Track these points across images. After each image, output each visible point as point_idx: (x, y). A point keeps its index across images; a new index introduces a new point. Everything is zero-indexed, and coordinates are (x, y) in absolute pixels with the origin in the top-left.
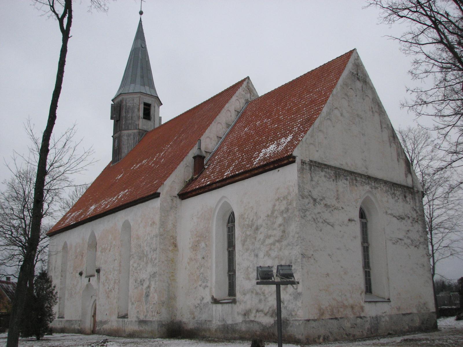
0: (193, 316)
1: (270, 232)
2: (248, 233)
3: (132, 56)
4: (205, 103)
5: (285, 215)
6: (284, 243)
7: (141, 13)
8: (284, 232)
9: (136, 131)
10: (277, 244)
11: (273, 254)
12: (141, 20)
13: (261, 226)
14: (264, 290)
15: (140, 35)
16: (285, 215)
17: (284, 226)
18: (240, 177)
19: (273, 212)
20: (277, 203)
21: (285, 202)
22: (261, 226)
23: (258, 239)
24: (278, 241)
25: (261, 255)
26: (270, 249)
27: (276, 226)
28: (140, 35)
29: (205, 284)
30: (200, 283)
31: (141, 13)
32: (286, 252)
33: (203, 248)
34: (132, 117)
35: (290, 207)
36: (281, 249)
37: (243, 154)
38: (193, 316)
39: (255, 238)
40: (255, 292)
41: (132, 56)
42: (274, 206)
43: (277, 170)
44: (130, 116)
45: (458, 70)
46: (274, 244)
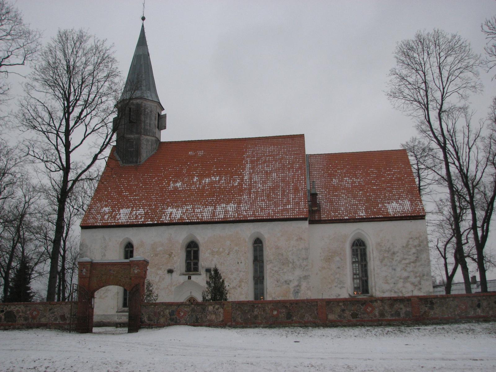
0: (210, 308)
1: (405, 257)
2: (386, 255)
3: (135, 59)
4: (259, 138)
5: (418, 248)
6: (418, 264)
7: (143, 19)
8: (417, 257)
9: (154, 138)
10: (412, 264)
11: (409, 269)
12: (143, 26)
13: (398, 252)
14: (402, 290)
15: (142, 42)
16: (418, 248)
17: (417, 254)
18: (379, 220)
19: (407, 245)
20: (411, 240)
21: (417, 241)
22: (398, 252)
23: (395, 260)
24: (413, 262)
25: (398, 269)
26: (407, 266)
27: (411, 253)
28: (142, 42)
29: (341, 285)
30: (335, 284)
31: (143, 19)
32: (420, 269)
34: (150, 124)
35: (421, 244)
36: (415, 267)
37: (215, 174)
38: (210, 308)
39: (393, 259)
40: (393, 291)
41: (135, 59)
42: (408, 241)
43: (411, 221)
44: (148, 123)
45: (103, 57)
46: (410, 264)
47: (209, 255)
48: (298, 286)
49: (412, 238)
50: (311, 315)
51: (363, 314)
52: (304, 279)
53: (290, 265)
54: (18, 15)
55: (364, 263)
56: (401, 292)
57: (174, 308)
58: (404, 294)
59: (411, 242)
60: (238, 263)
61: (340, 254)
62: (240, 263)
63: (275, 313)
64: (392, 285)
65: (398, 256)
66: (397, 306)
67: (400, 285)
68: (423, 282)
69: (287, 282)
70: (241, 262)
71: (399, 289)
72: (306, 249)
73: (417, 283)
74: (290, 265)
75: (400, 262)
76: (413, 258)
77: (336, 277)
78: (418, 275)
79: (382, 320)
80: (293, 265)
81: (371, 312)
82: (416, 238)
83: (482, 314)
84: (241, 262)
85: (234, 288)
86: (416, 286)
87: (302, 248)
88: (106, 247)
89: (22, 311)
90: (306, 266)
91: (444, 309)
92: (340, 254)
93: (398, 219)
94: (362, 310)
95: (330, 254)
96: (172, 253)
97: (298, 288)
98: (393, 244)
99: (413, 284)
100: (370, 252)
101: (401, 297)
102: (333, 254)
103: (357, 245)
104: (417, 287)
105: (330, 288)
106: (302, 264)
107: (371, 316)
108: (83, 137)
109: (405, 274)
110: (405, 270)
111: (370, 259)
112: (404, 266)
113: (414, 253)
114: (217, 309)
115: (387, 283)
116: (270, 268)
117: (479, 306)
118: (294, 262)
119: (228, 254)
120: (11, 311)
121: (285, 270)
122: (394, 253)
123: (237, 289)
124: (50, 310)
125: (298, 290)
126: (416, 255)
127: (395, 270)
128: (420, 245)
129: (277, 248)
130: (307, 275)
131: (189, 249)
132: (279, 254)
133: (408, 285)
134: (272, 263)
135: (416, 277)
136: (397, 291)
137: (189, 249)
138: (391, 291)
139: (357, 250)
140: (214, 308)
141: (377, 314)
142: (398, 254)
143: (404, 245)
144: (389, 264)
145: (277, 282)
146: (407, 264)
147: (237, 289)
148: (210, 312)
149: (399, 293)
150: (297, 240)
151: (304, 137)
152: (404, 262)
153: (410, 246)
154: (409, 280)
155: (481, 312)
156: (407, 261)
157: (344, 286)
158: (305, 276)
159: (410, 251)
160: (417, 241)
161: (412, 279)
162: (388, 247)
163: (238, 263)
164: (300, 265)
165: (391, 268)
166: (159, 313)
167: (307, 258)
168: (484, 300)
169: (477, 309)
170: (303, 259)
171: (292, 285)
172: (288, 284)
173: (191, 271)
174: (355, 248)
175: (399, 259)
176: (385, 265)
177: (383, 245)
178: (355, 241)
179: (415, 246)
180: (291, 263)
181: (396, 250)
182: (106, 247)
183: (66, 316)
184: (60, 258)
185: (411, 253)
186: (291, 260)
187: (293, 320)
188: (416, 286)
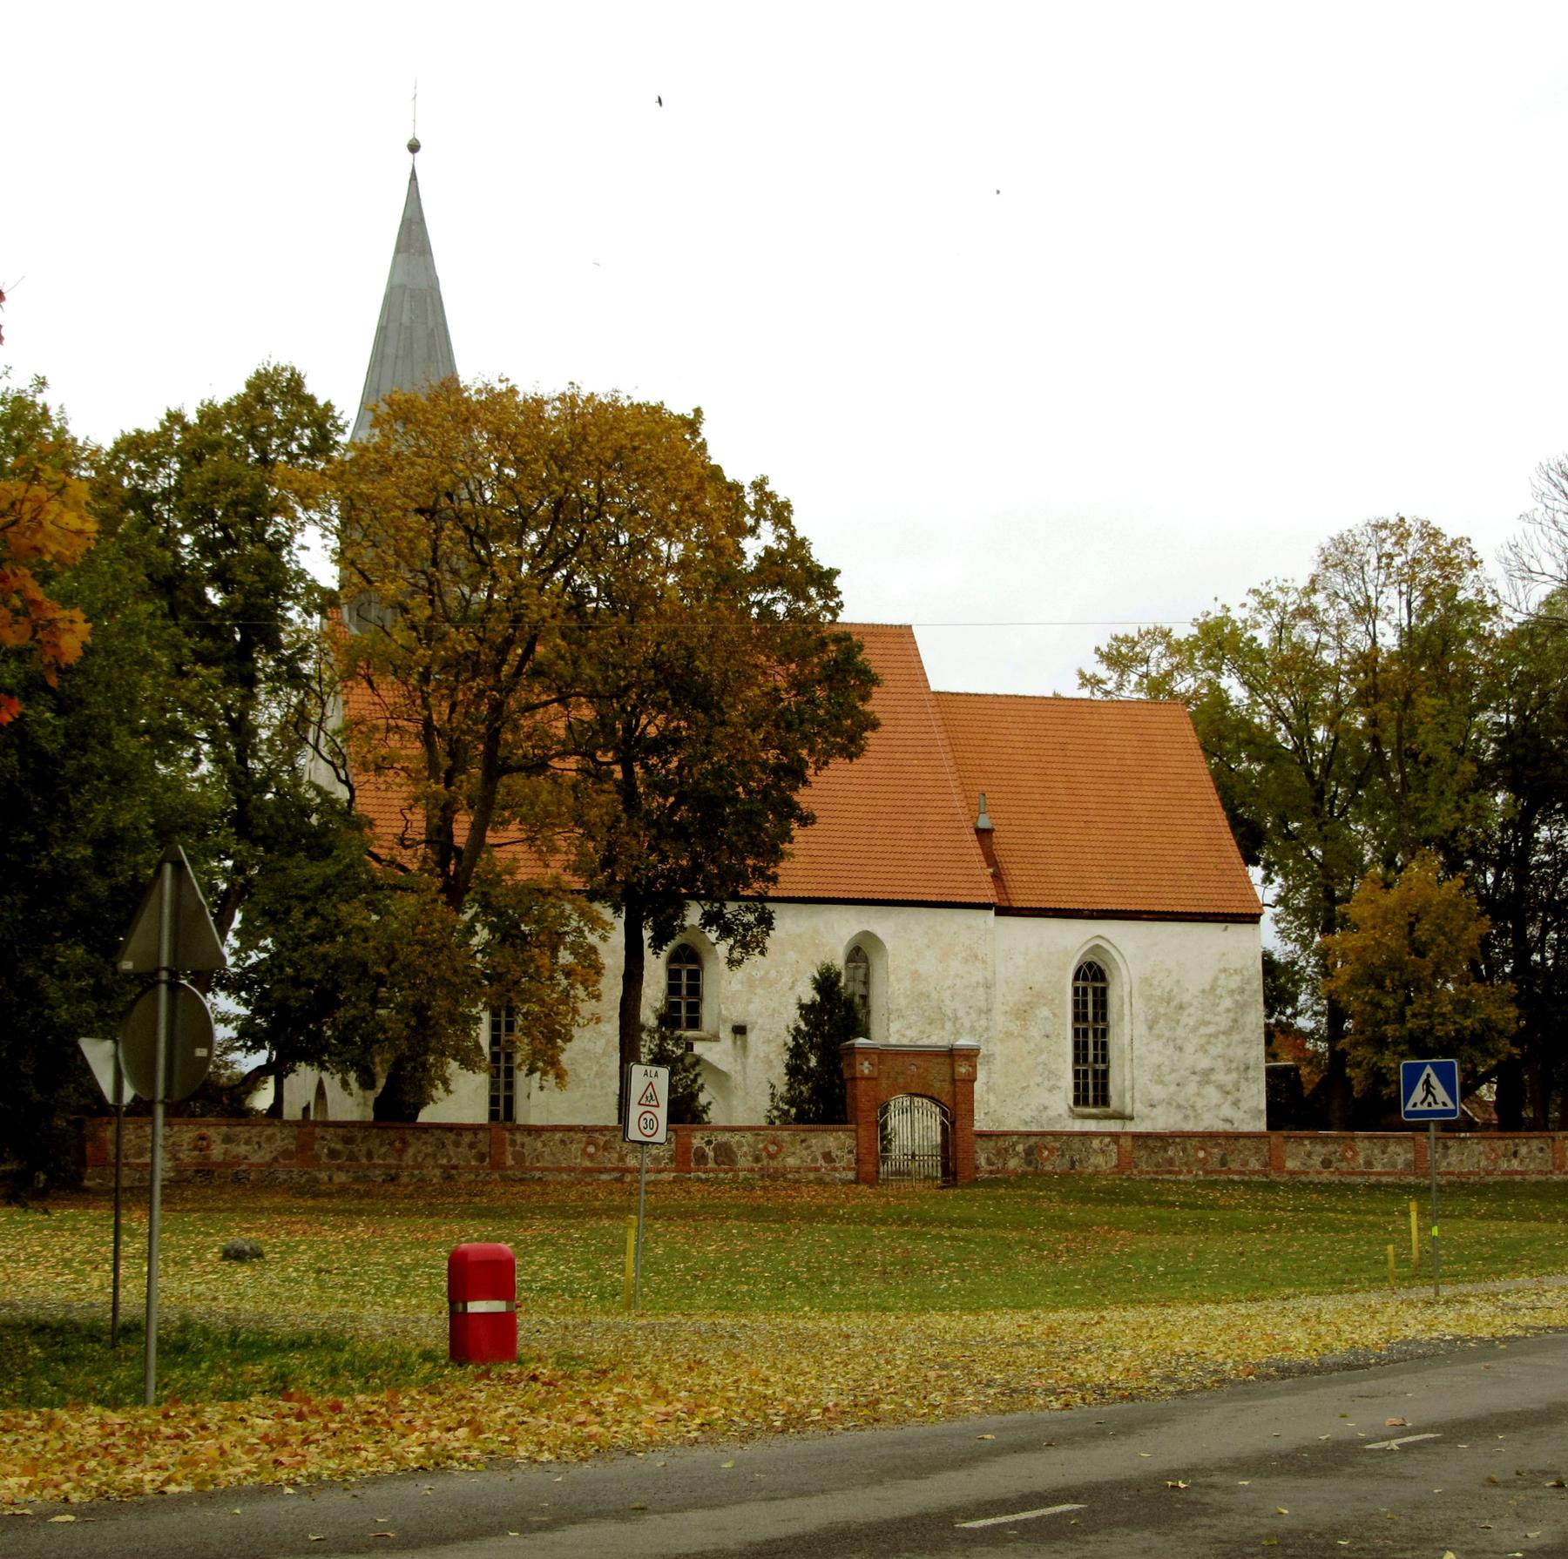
1: (1209, 1017)
2: (1161, 1010)
5: (1238, 998)
6: (1236, 1037)
10: (1222, 1037)
11: (1214, 1051)
20: (1223, 976)
21: (1237, 978)
25: (1190, 1049)
26: (1209, 1043)
29: (1052, 1083)
30: (1038, 1079)
33: (1047, 1018)
35: (1247, 987)
36: (1229, 1046)
42: (1216, 979)
46: (1216, 1035)
47: (739, 987)
49: (1225, 970)
51: (1341, 1161)
53: (948, 1025)
54: (616, 400)
55: (1100, 1026)
57: (1033, 1140)
59: (1222, 982)
61: (1052, 1000)
63: (1201, 1154)
64: (1173, 1088)
65: (1189, 1015)
67: (1192, 1088)
68: (1243, 1085)
71: (1188, 1100)
72: (988, 986)
73: (1229, 1087)
75: (1194, 1030)
76: (1225, 1022)
77: (1040, 1059)
78: (1234, 1065)
80: (954, 1024)
81: (1353, 1157)
82: (1236, 971)
86: (1228, 1093)
89: (748, 1142)
90: (987, 1029)
92: (1052, 1000)
95: (1028, 999)
98: (1178, 981)
99: (1220, 1087)
100: (1122, 998)
102: (1035, 1000)
103: (1085, 979)
104: (1229, 1097)
105: (1023, 1088)
106: (976, 1024)
109: (1204, 1063)
110: (1206, 1052)
111: (1122, 1018)
112: (1203, 1041)
113: (1228, 1010)
115: (1162, 1083)
117: (1515, 1154)
118: (956, 1018)
119: (791, 989)
120: (725, 1143)
122: (1181, 1007)
124: (803, 1141)
126: (1232, 1015)
127: (1181, 1049)
128: (1242, 991)
129: (916, 976)
131: (675, 966)
132: (921, 994)
133: (1211, 1092)
135: (1229, 1071)
136: (1183, 1103)
137: (675, 966)
138: (1169, 1104)
139: (1085, 990)
141: (1361, 1162)
142: (1191, 1010)
143: (1207, 987)
144: (1167, 1034)
146: (1210, 1036)
148: (1095, 1151)
150: (966, 960)
151: (912, 635)
152: (1203, 1030)
153: (1219, 991)
154: (1213, 1077)
156: (1211, 1029)
157: (1059, 1084)
159: (1218, 1005)
160: (1237, 978)
161: (1220, 1077)
162: (1167, 989)
165: (1172, 1044)
166: (1006, 1150)
167: (989, 1010)
170: (980, 1012)
173: (1086, 1103)
174: (1080, 984)
175: (1191, 1022)
176: (1159, 1037)
177: (1156, 983)
178: (1081, 967)
179: (1232, 992)
181: (1186, 998)
183: (834, 1155)
184: (1127, 1063)
185: (1220, 1009)
186: (949, 1013)
188: (1228, 1093)
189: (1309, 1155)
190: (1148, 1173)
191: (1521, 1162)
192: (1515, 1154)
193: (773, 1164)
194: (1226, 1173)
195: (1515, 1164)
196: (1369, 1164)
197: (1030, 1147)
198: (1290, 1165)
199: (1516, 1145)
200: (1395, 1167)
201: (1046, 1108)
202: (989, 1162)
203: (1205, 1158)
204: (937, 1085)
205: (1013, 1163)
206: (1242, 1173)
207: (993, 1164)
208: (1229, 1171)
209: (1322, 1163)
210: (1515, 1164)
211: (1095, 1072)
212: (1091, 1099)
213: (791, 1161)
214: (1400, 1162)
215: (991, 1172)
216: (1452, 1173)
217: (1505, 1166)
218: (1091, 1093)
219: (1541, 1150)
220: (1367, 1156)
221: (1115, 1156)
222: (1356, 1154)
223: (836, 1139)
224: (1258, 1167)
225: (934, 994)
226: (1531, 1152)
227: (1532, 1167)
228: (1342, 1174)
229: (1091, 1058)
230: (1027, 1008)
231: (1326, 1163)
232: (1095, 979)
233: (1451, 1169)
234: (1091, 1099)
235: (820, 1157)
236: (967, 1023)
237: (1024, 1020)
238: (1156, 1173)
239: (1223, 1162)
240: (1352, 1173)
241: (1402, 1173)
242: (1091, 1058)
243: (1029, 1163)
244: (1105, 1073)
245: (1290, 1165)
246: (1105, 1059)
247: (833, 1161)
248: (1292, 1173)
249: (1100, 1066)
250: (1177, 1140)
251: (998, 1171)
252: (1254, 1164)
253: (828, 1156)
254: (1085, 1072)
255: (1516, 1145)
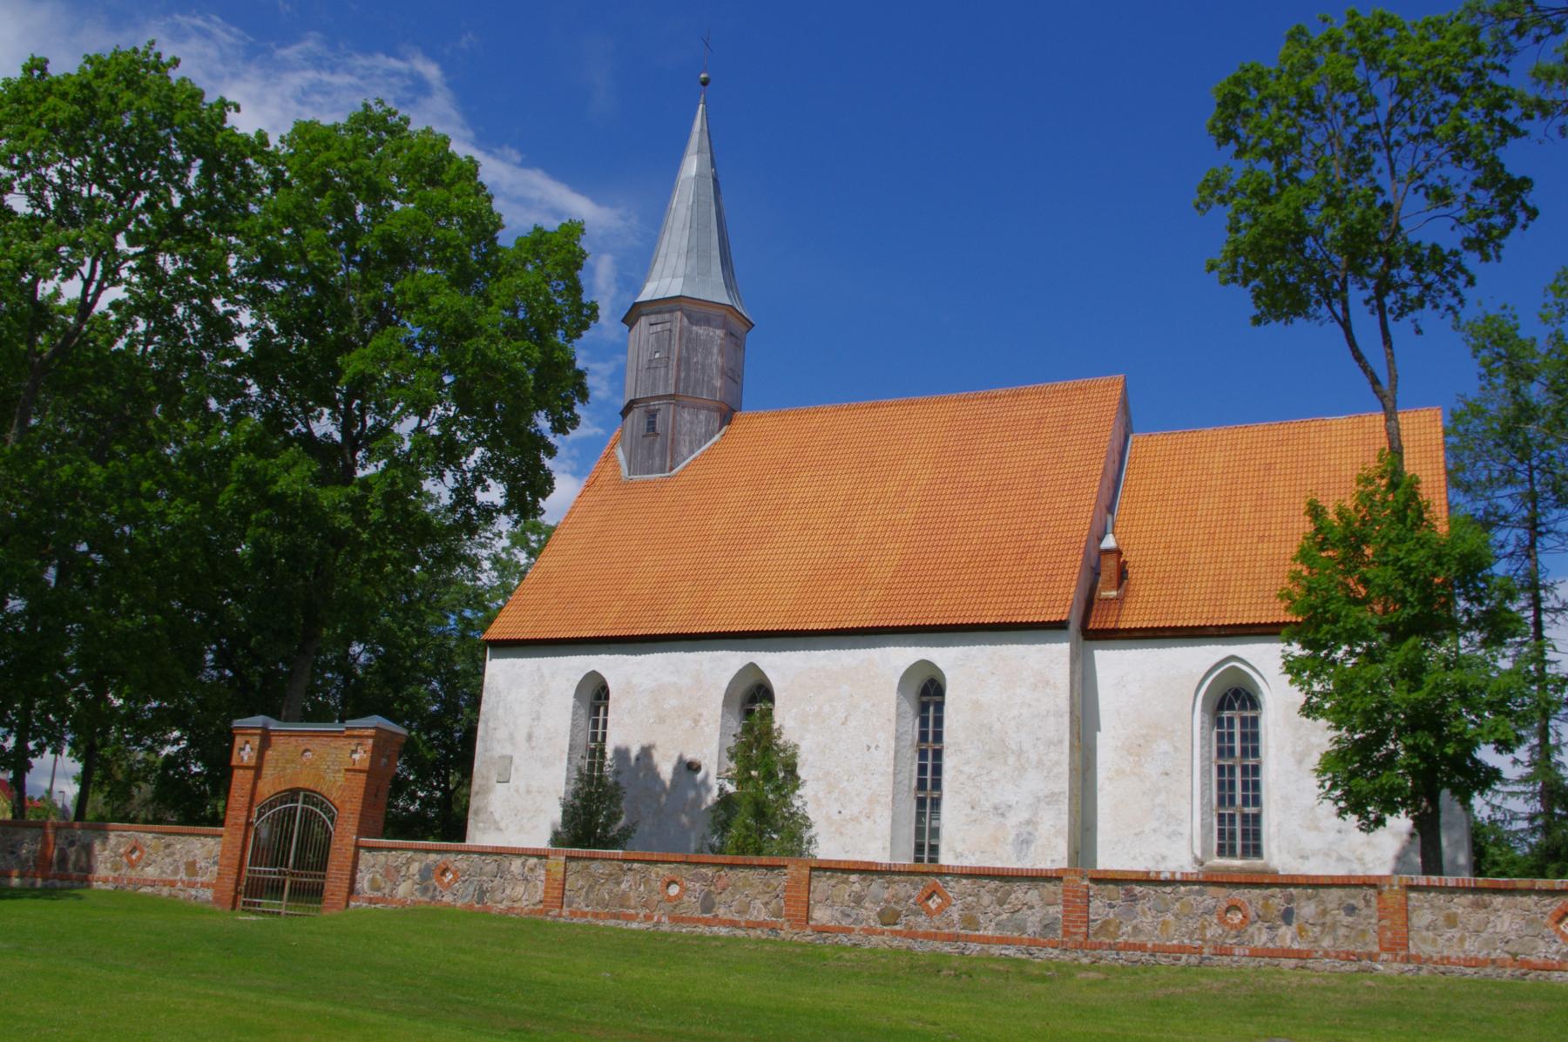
33: (1166, 753)
34: (703, 366)
40: (1334, 855)
48: (1028, 822)
50: (766, 904)
51: (917, 913)
52: (1048, 803)
53: (1012, 759)
55: (1251, 762)
56: (1360, 860)
58: (1371, 865)
60: (869, 748)
62: (873, 749)
66: (1020, 895)
69: (1000, 811)
70: (877, 747)
74: (1012, 759)
79: (968, 939)
81: (940, 909)
83: (1296, 946)
84: (877, 747)
85: (855, 819)
87: (1048, 712)
88: (542, 696)
91: (1169, 917)
93: (1265, 630)
94: (912, 901)
95: (1144, 731)
96: (700, 715)
97: (1030, 828)
101: (1359, 877)
107: (938, 923)
108: (1341, 332)
114: (532, 870)
115: (1317, 828)
116: (955, 767)
117: (1287, 917)
121: (995, 775)
123: (860, 823)
125: (1030, 834)
130: (1057, 790)
134: (961, 751)
136: (1346, 854)
138: (1327, 855)
140: (524, 865)
141: (956, 916)
145: (973, 808)
147: (860, 823)
149: (1349, 861)
155: (1293, 940)
158: (1053, 794)
163: (869, 748)
164: (1040, 763)
168: (1309, 898)
169: (1279, 926)
171: (1013, 820)
172: (1003, 815)
173: (1232, 854)
178: (1226, 695)
180: (1013, 752)
182: (542, 696)
186: (1013, 746)
187: (716, 916)
189: (858, 900)
190: (584, 915)
191: (1301, 931)
192: (1287, 917)
193: (133, 874)
194: (707, 923)
195: (1287, 936)
196: (970, 921)
197: (427, 866)
198: (821, 915)
199: (1290, 899)
200: (1023, 930)
201: (1164, 858)
202: (375, 887)
203: (678, 897)
204: (330, 776)
205: (403, 889)
206: (733, 924)
207: (378, 889)
208: (717, 921)
209: (881, 914)
210: (1287, 936)
211: (1245, 817)
212: (1239, 850)
213: (151, 872)
214: (1033, 922)
215: (370, 901)
216: (1142, 947)
217: (1261, 938)
218: (1239, 842)
219: (1351, 910)
220: (967, 907)
221: (541, 886)
222: (947, 902)
223: (204, 845)
224: (763, 916)
225: (997, 726)
226: (1324, 913)
227: (1326, 943)
228: (911, 934)
229: (1238, 800)
230: (1142, 741)
231: (889, 917)
232: (1243, 707)
233: (1142, 938)
234: (1239, 850)
235: (182, 868)
236: (1033, 756)
237: (1138, 756)
238: (596, 915)
239: (708, 905)
240: (934, 937)
241: (1033, 942)
242: (1238, 800)
243: (425, 890)
244: (1257, 818)
245: (821, 915)
246: (1257, 801)
247: (195, 874)
248: (821, 930)
249: (1250, 810)
250: (636, 865)
251: (383, 899)
252: (759, 913)
253: (191, 867)
254: (1232, 816)
255: (1290, 899)
